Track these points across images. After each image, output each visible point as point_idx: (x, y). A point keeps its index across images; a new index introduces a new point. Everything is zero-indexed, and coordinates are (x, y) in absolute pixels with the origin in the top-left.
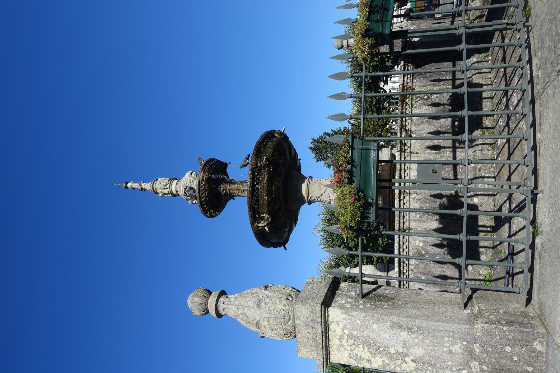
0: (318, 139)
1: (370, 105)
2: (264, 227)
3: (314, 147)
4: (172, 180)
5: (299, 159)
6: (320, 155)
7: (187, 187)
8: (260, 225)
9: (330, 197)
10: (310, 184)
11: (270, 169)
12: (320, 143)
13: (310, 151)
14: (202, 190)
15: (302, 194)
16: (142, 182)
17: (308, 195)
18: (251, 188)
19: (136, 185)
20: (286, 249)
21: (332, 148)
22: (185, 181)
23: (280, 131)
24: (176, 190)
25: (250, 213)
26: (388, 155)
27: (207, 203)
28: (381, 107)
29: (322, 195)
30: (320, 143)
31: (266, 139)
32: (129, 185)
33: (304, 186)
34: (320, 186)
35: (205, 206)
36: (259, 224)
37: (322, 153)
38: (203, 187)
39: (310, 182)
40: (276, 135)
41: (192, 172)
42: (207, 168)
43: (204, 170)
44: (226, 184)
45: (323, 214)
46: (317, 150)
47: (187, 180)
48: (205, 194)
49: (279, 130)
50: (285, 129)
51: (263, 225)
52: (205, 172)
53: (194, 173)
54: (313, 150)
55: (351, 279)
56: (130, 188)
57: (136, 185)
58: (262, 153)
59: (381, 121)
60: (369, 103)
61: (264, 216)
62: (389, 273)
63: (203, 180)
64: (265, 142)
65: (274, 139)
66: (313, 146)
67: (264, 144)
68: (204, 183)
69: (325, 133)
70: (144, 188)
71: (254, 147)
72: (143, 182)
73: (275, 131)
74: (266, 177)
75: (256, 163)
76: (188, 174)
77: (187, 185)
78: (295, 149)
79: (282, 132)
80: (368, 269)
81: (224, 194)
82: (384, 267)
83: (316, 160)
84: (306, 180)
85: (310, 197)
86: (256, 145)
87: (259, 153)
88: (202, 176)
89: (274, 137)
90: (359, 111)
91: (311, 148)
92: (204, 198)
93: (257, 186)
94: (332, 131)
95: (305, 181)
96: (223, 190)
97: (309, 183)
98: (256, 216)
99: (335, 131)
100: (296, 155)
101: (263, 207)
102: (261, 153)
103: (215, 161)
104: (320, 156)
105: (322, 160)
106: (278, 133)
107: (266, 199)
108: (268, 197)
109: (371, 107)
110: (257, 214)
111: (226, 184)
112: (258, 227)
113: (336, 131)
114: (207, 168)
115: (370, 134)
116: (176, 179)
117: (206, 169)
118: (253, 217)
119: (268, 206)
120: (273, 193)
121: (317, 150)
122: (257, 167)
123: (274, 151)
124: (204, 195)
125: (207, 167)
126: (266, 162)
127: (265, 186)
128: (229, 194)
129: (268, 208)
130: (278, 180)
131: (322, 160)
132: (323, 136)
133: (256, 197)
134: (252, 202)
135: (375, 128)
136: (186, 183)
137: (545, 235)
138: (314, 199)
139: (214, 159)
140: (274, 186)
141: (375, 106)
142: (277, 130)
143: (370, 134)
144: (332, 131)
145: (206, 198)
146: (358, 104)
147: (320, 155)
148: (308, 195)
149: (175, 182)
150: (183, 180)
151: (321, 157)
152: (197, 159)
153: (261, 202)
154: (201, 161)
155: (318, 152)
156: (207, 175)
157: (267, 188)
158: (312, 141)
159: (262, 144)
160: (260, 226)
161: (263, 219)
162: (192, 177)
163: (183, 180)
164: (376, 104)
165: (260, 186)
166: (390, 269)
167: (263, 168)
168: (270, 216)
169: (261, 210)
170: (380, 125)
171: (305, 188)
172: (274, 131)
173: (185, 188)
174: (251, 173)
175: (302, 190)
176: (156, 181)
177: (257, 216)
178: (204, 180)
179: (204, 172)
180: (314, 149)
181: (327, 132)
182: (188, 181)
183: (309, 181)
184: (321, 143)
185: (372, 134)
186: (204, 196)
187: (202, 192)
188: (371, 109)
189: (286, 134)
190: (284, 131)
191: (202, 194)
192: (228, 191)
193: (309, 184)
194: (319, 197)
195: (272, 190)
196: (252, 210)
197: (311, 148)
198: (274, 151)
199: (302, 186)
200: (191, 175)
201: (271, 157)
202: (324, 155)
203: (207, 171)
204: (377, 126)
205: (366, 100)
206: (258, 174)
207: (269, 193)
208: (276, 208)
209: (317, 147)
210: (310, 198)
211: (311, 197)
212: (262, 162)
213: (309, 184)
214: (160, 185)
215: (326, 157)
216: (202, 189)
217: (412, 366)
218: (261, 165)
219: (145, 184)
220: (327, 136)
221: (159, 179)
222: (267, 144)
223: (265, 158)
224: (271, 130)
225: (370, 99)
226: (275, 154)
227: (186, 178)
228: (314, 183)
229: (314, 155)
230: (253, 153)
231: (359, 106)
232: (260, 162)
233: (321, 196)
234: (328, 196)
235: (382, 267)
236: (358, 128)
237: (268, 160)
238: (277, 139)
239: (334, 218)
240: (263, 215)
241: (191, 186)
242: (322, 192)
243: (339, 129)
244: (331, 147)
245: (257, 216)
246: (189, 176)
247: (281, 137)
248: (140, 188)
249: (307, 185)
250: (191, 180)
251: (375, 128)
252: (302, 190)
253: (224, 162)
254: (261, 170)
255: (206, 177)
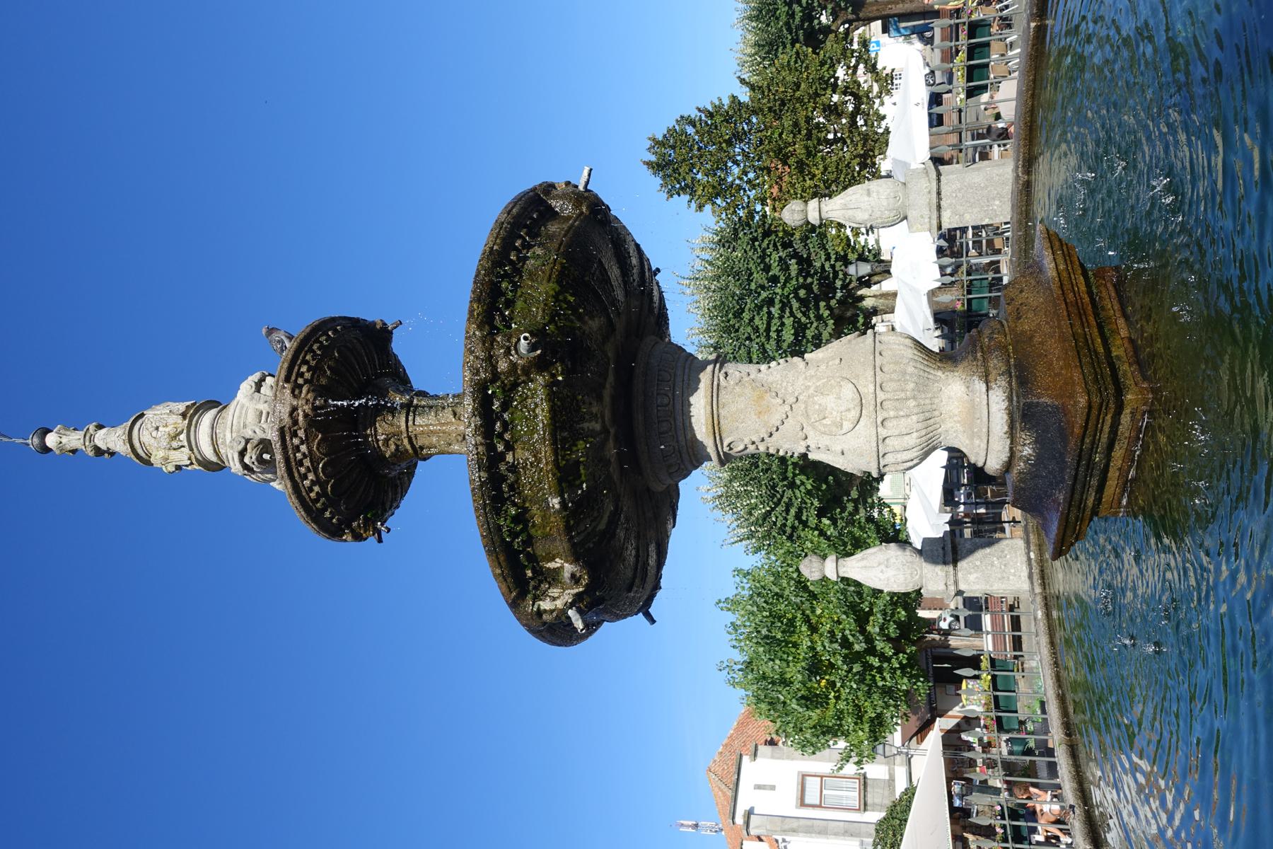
0: (665, 136)
1: (787, 24)
2: (563, 612)
3: (658, 159)
4: (191, 415)
5: (654, 269)
6: (675, 178)
7: (247, 441)
8: (546, 605)
9: (806, 438)
10: (722, 392)
11: (553, 376)
12: (670, 146)
13: (647, 173)
14: (301, 460)
15: (694, 435)
16: (92, 427)
17: (718, 438)
18: (482, 474)
19: (73, 440)
20: (653, 621)
21: (704, 157)
22: (240, 417)
23: (570, 189)
24: (217, 453)
25: (498, 571)
26: (929, 192)
27: (331, 503)
28: (817, 27)
29: (776, 435)
30: (670, 146)
31: (521, 237)
32: (51, 440)
33: (699, 405)
34: (761, 398)
35: (327, 514)
36: (541, 603)
37: (679, 174)
38: (303, 448)
39: (718, 385)
40: (556, 204)
41: (262, 380)
42: (304, 369)
43: (293, 378)
44: (393, 417)
45: (702, 333)
46: (665, 166)
47: (246, 414)
48: (316, 474)
49: (568, 183)
50: (589, 175)
51: (559, 604)
52: (300, 387)
53: (269, 380)
54: (657, 167)
55: (785, 483)
56: (58, 452)
57: (73, 440)
58: (510, 304)
59: (829, 68)
60: (784, 18)
61: (559, 565)
62: (959, 564)
63: (295, 422)
64: (516, 249)
65: (553, 228)
66: (653, 158)
67: (511, 263)
68: (301, 433)
69: (682, 117)
70: (104, 447)
71: (470, 286)
72: (100, 427)
73: (552, 186)
74: (542, 414)
75: (490, 360)
76: (246, 387)
77: (249, 434)
78: (637, 246)
79: (581, 188)
80: (893, 560)
81: (393, 455)
82: (943, 548)
83: (666, 195)
84: (705, 377)
85: (725, 444)
86: (477, 276)
87: (498, 309)
88: (288, 409)
89: (551, 214)
90: (759, 46)
91: (649, 164)
92: (316, 489)
93: (509, 458)
94: (699, 110)
95: (699, 381)
96: (386, 441)
97: (715, 391)
98: (526, 575)
99: (709, 111)
100: (646, 267)
101: (546, 536)
102: (507, 308)
103: (335, 331)
104: (676, 182)
105: (681, 192)
106: (563, 196)
107: (557, 506)
108: (562, 497)
109: (790, 30)
110: (525, 567)
111: (393, 417)
112: (540, 613)
113: (711, 110)
114: (304, 369)
115: (802, 106)
116: (212, 404)
117: (301, 375)
118: (514, 582)
119: (568, 529)
120: (582, 471)
121: (665, 166)
122: (495, 376)
123: (558, 288)
124: (311, 476)
125: (306, 362)
126: (533, 348)
127: (546, 452)
128: (411, 451)
129: (571, 538)
130: (594, 410)
131: (681, 192)
132: (677, 127)
133: (514, 504)
134: (499, 528)
135: (814, 87)
136: (245, 426)
137: (786, 126)
138: (741, 447)
139: (333, 319)
140: (581, 444)
141: (801, 27)
142: (559, 180)
143: (802, 106)
144: (699, 110)
145: (323, 488)
146: (755, 25)
147: (675, 178)
148: (718, 438)
149: (208, 417)
150: (230, 417)
151: (678, 186)
152: (264, 331)
153: (537, 520)
154: (279, 342)
155: (669, 171)
156: (307, 401)
157: (556, 463)
158: (649, 143)
159: (502, 265)
160: (545, 611)
161: (554, 578)
162: (262, 401)
163: (230, 417)
164: (802, 21)
165: (522, 455)
166: (959, 552)
167: (523, 378)
168: (582, 567)
169: (540, 549)
170: (826, 79)
171: (702, 411)
172: (549, 188)
173: (240, 447)
174: (474, 409)
175: (693, 420)
176: (140, 421)
177: (529, 573)
178: (301, 418)
179: (293, 392)
180: (658, 165)
181: (686, 115)
182: (251, 417)
183: (715, 383)
184: (673, 147)
185: (807, 108)
186: (313, 483)
187: (303, 470)
188: (791, 34)
189: (596, 196)
190: (587, 183)
191: (305, 477)
192: (406, 441)
193: (718, 397)
194: (763, 440)
195: (578, 463)
196: (502, 558)
197: (649, 164)
198: (558, 288)
199: (690, 405)
200: (258, 390)
201: (552, 321)
202: (684, 179)
203: (306, 381)
204: (820, 84)
205: (775, 13)
206: (506, 406)
207: (566, 477)
208: (602, 526)
209: (664, 160)
210: (726, 449)
211: (729, 445)
212: (517, 352)
213: (718, 397)
214: (154, 434)
215: (692, 182)
216: (299, 455)
217: (1064, 846)
218: (513, 366)
219: (103, 431)
220: (687, 127)
221: (149, 414)
222: (526, 258)
223: (525, 338)
224: (534, 190)
225: (787, 8)
226: (568, 302)
227: (243, 406)
228: (738, 389)
229: (658, 181)
230: (471, 312)
231: (759, 29)
232: (508, 353)
233: (771, 435)
234: (801, 435)
235: (937, 550)
236: (766, 94)
237: (539, 338)
238: (565, 226)
239: (730, 341)
240: (551, 565)
241: (263, 436)
242: (775, 420)
243: (717, 103)
244: (701, 156)
245: (529, 573)
246: (252, 399)
247: (582, 213)
248: (89, 449)
249: (710, 400)
250: (261, 413)
251: (814, 87)
252: (690, 423)
253: (374, 324)
254: (515, 385)
255: (304, 408)
